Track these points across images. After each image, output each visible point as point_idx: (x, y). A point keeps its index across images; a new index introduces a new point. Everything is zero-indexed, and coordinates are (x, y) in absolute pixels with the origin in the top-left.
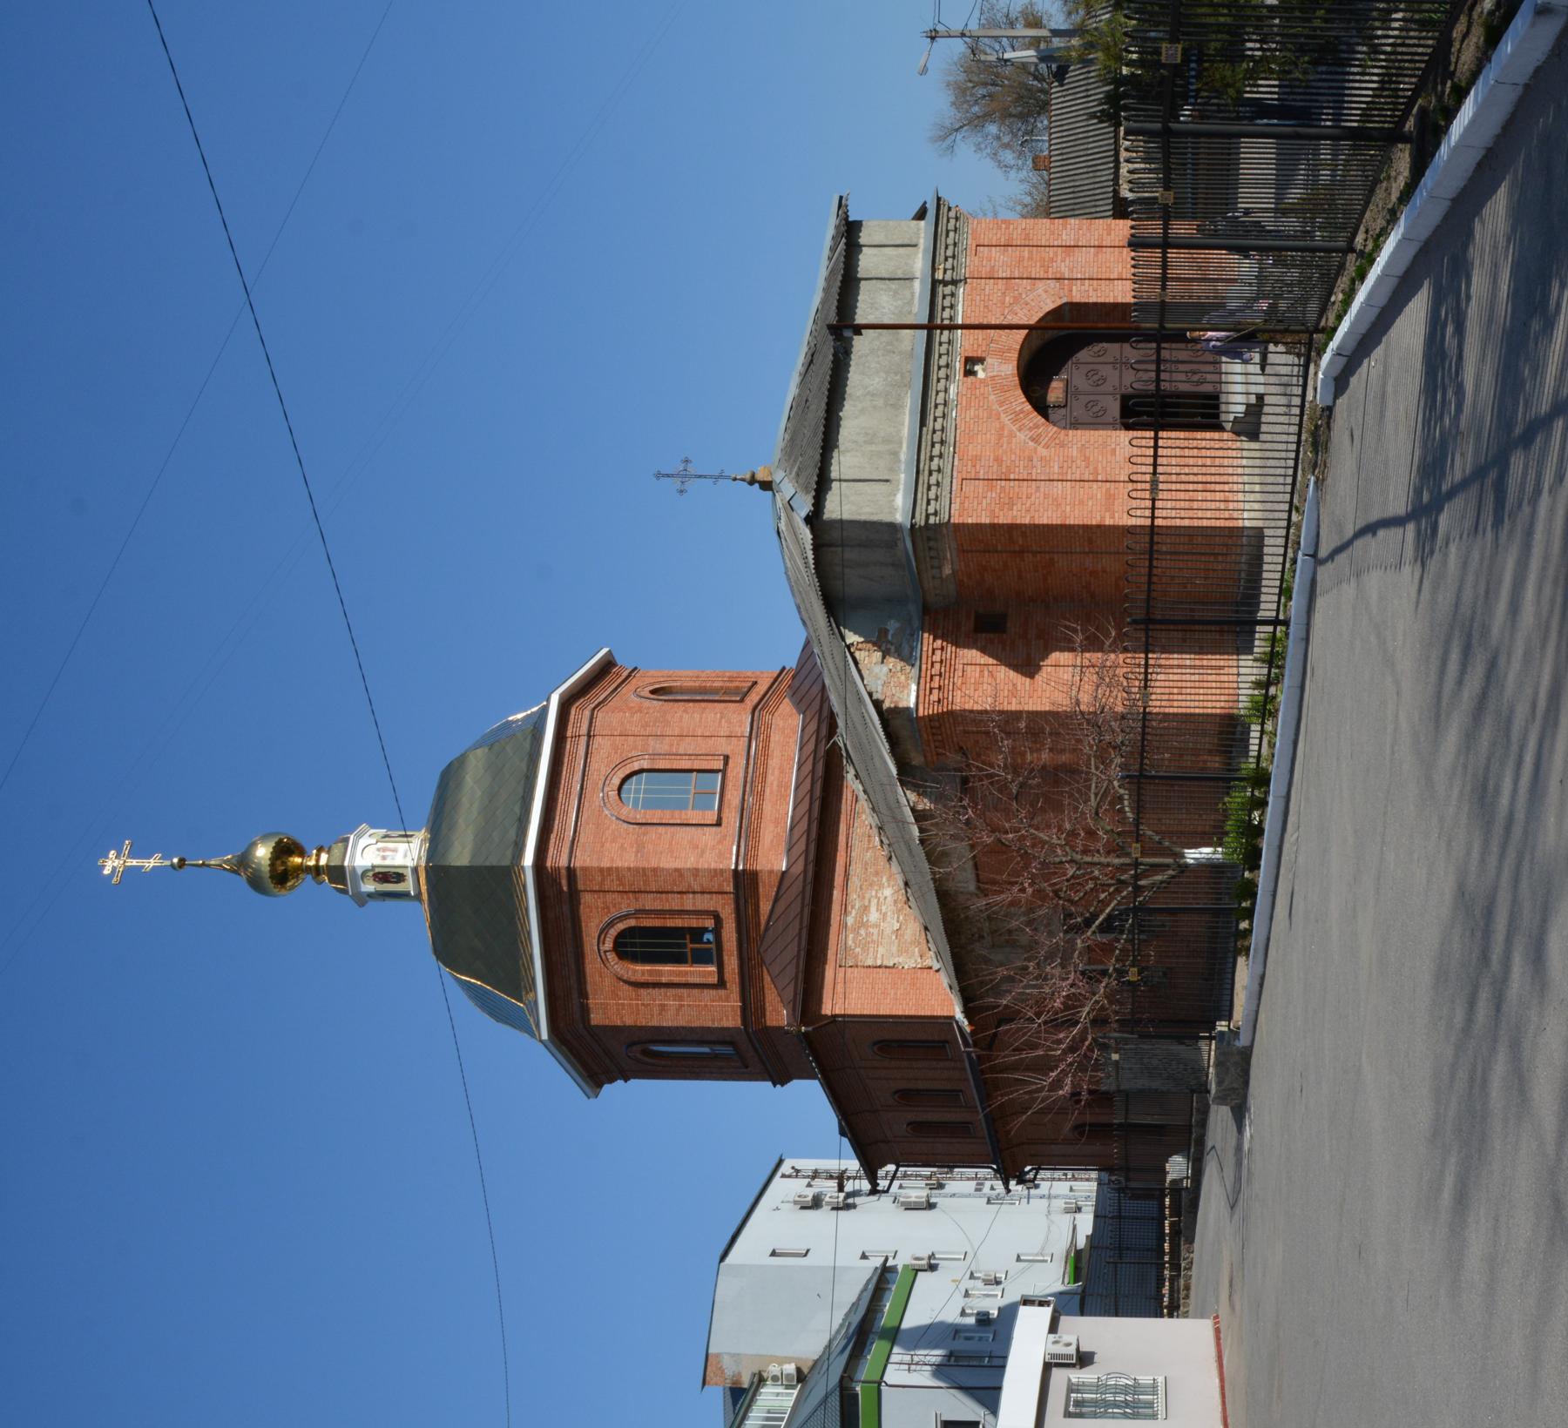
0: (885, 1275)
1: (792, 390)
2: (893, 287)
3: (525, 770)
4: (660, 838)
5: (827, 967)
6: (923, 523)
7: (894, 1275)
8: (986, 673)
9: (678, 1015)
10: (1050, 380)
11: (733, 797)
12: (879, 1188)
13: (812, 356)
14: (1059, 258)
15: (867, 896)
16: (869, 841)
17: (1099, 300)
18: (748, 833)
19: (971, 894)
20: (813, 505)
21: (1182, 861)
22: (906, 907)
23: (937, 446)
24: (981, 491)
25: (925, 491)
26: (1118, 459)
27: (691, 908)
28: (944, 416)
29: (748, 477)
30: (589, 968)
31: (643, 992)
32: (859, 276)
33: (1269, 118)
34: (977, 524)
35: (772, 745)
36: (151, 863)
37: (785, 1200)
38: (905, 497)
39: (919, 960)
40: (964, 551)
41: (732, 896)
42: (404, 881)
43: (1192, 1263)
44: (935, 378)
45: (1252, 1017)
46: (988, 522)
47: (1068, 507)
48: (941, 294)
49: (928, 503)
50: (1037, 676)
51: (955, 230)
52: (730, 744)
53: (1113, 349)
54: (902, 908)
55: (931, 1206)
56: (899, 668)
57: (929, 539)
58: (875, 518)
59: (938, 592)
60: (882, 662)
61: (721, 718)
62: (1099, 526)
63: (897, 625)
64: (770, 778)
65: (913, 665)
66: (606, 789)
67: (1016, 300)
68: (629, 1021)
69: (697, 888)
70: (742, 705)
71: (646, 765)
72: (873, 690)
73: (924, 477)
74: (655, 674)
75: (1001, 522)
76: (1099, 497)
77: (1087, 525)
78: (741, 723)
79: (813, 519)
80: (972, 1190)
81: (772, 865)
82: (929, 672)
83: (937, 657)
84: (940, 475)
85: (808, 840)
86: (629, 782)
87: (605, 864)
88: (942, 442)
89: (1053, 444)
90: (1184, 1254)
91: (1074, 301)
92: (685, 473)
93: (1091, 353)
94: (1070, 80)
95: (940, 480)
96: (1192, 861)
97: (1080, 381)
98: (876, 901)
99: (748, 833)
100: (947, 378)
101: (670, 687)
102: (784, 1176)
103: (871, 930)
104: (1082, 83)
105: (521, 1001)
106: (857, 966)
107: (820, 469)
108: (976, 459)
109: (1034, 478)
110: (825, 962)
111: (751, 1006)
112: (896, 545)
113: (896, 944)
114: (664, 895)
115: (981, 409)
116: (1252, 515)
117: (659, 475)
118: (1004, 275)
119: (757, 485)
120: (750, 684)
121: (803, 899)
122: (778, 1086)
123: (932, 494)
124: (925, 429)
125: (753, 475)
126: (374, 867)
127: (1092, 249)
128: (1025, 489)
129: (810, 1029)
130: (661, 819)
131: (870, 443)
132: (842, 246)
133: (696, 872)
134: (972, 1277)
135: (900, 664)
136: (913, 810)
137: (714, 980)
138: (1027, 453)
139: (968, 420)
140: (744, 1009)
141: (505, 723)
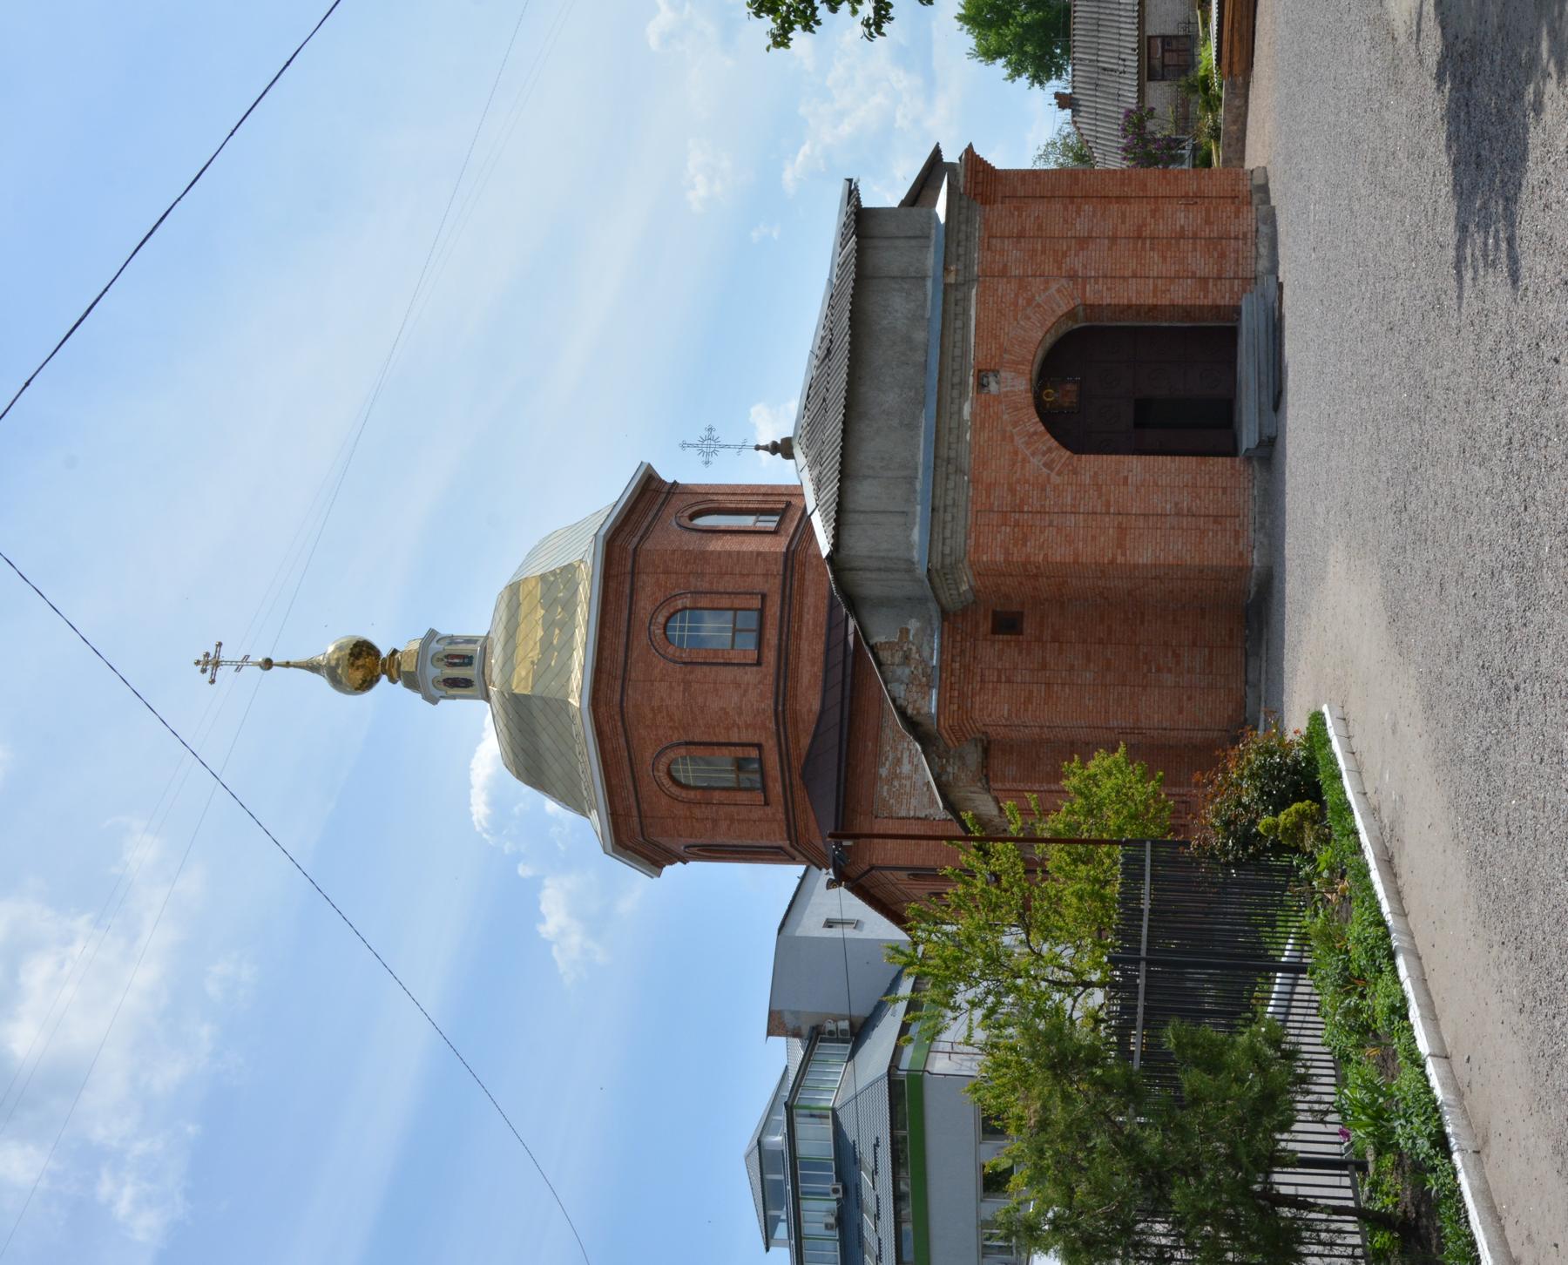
2: (906, 286)
15: (900, 747)
27: (737, 741)
33: (1341, 1169)
35: (807, 583)
42: (472, 685)
63: (918, 624)
64: (806, 617)
72: (897, 695)
84: (955, 510)
89: (1066, 472)
103: (904, 781)
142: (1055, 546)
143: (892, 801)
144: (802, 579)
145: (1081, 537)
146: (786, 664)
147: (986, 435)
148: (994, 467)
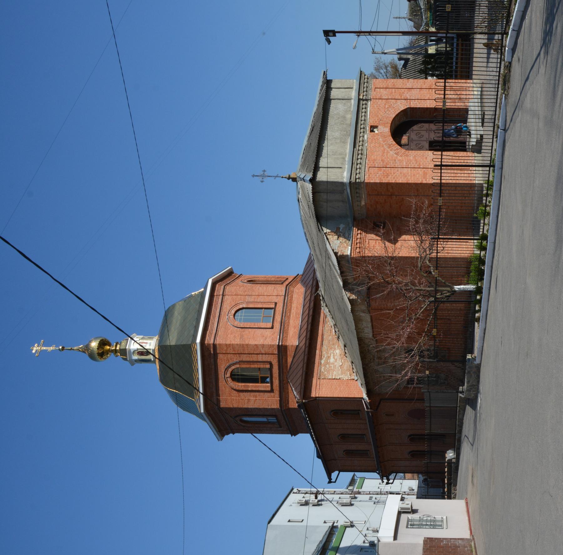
0: (333, 529)
1: (305, 143)
2: (344, 102)
3: (200, 301)
4: (249, 333)
5: (314, 379)
6: (354, 181)
7: (337, 529)
8: (377, 243)
9: (255, 403)
10: (402, 136)
11: (278, 318)
12: (332, 481)
13: (313, 128)
14: (406, 92)
15: (330, 353)
16: (331, 332)
17: (421, 107)
18: (283, 331)
19: (370, 339)
20: (313, 175)
21: (453, 289)
22: (345, 357)
23: (360, 155)
24: (376, 171)
25: (355, 170)
26: (428, 160)
28: (362, 145)
29: (287, 176)
30: (220, 384)
31: (241, 394)
32: (331, 98)
34: (375, 183)
35: (293, 299)
36: (51, 348)
37: (294, 502)
38: (347, 173)
39: (349, 376)
40: (369, 195)
41: (277, 355)
43: (456, 495)
44: (359, 132)
45: (481, 349)
46: (379, 182)
47: (409, 177)
48: (361, 104)
49: (356, 174)
50: (397, 244)
51: (367, 82)
52: (277, 298)
53: (426, 126)
54: (343, 357)
55: (352, 505)
56: (344, 241)
57: (356, 188)
58: (336, 180)
59: (359, 212)
60: (338, 239)
61: (274, 289)
62: (421, 184)
63: (344, 226)
64: (293, 311)
65: (349, 240)
66: (229, 315)
67: (390, 106)
68: (235, 406)
69: (263, 352)
70: (282, 285)
71: (245, 306)
72: (334, 248)
73: (355, 165)
74: (248, 275)
75: (384, 182)
76: (421, 173)
77: (416, 183)
78: (282, 290)
79: (313, 181)
80: (368, 499)
81: (293, 343)
82: (355, 242)
83: (359, 236)
84: (361, 165)
85: (304, 354)
86: (238, 312)
87: (228, 342)
88: (362, 154)
90: (453, 491)
91: (412, 107)
92: (263, 175)
93: (418, 127)
94: (409, 67)
95: (361, 167)
96: (457, 289)
97: (413, 136)
98: (333, 354)
99: (283, 331)
100: (364, 132)
101: (255, 280)
102: (294, 493)
104: (413, 67)
105: (193, 398)
106: (325, 379)
107: (315, 163)
108: (374, 160)
109: (396, 167)
110: (313, 377)
111: (283, 399)
112: (344, 192)
113: (341, 371)
114: (250, 355)
115: (376, 143)
116: (479, 179)
117: (254, 176)
118: (385, 98)
119: (291, 180)
120: (285, 279)
121: (301, 385)
122: (293, 436)
123: (358, 172)
124: (355, 149)
125: (289, 176)
126: (138, 349)
127: (418, 89)
128: (393, 171)
129: (307, 401)
130: (250, 326)
131: (334, 155)
132: (325, 87)
133: (263, 346)
134: (368, 529)
135: (344, 240)
136: (348, 298)
137: (269, 389)
138: (393, 158)
139: (371, 147)
140: (280, 401)
141: (190, 295)
142: (399, 178)
143: (326, 373)
144: (292, 297)
145: (409, 174)
146: (284, 328)
147: (373, 145)
148: (376, 154)
